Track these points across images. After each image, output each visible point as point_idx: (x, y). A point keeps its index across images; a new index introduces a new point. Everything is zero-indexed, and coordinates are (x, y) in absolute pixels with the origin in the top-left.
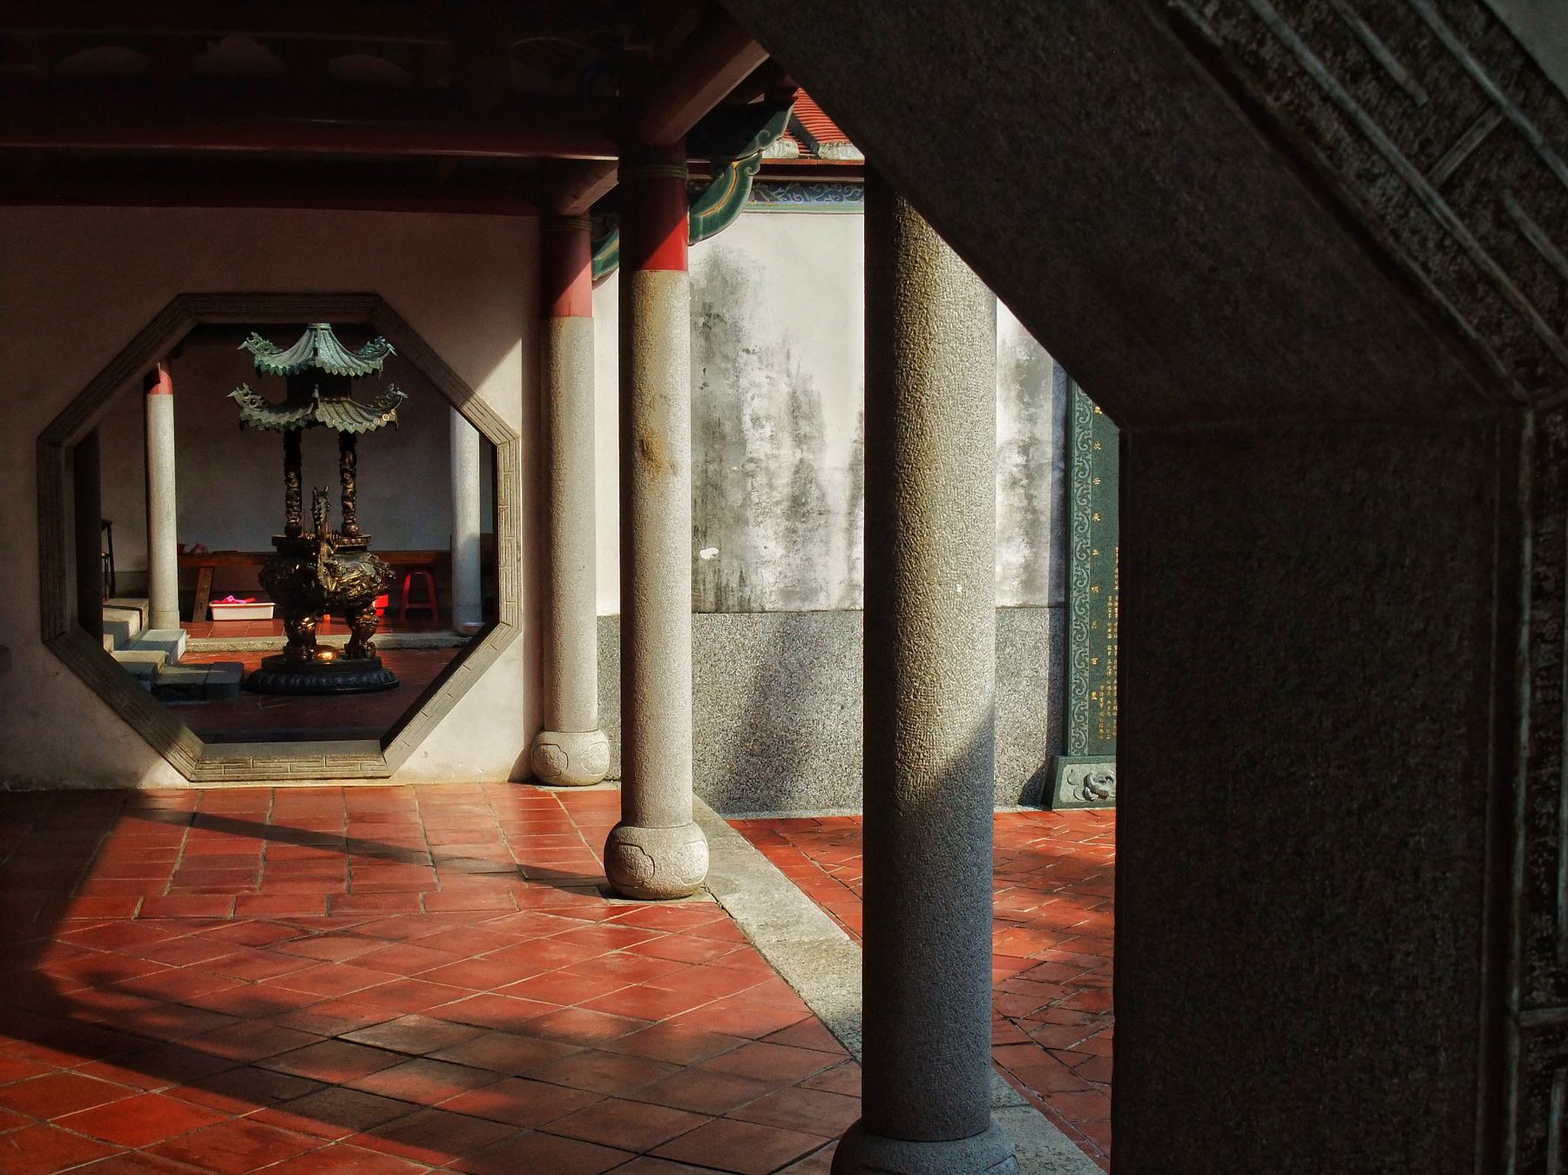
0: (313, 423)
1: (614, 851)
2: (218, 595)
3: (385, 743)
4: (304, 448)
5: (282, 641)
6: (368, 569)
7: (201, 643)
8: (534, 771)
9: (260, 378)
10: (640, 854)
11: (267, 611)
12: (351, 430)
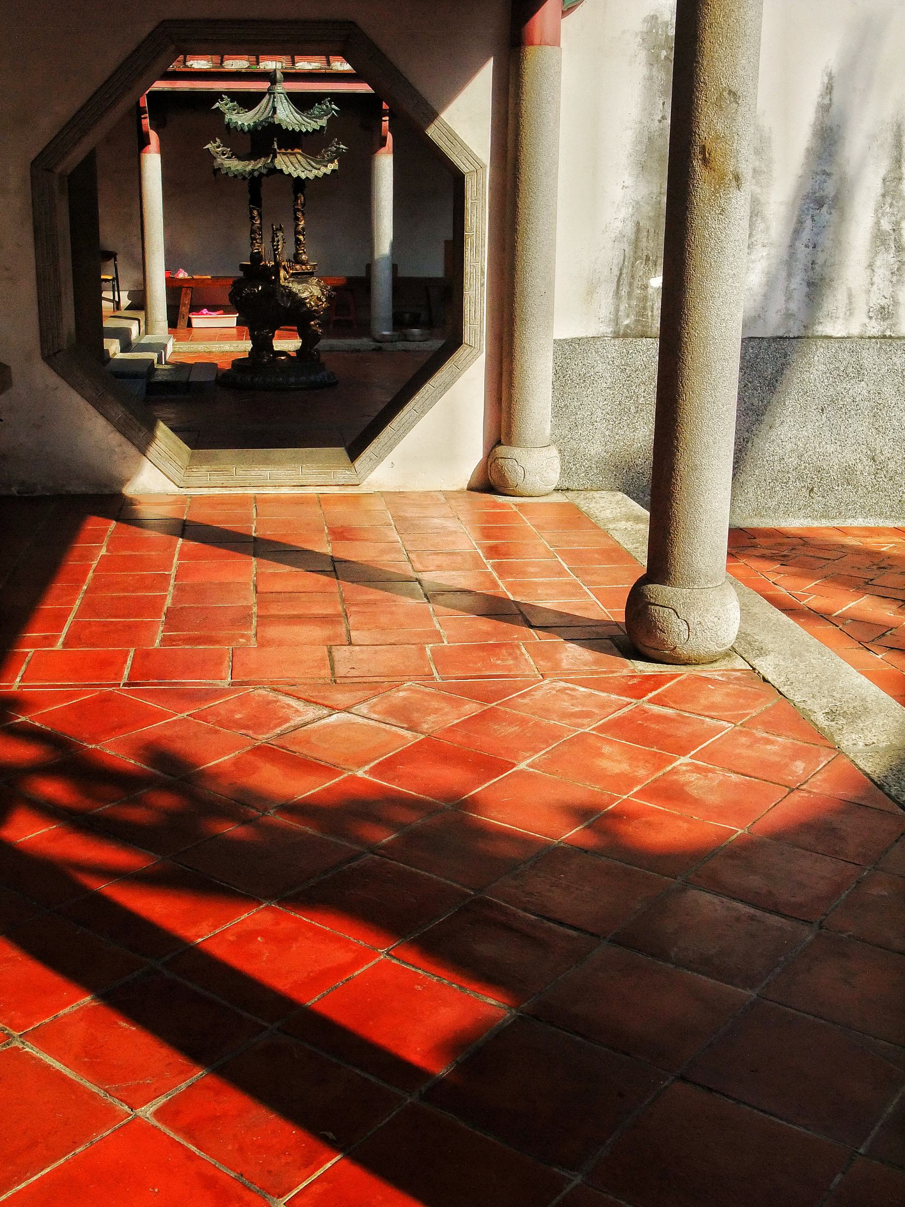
0: (274, 171)
1: (637, 603)
2: (196, 308)
3: (354, 452)
4: (264, 192)
5: (248, 345)
6: (317, 292)
7: (184, 346)
8: (490, 482)
9: (230, 134)
10: (674, 617)
11: (231, 320)
12: (303, 176)
